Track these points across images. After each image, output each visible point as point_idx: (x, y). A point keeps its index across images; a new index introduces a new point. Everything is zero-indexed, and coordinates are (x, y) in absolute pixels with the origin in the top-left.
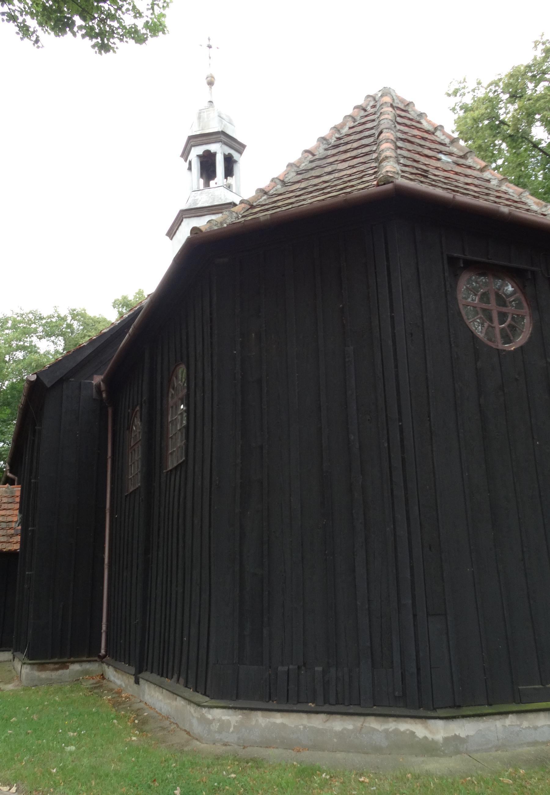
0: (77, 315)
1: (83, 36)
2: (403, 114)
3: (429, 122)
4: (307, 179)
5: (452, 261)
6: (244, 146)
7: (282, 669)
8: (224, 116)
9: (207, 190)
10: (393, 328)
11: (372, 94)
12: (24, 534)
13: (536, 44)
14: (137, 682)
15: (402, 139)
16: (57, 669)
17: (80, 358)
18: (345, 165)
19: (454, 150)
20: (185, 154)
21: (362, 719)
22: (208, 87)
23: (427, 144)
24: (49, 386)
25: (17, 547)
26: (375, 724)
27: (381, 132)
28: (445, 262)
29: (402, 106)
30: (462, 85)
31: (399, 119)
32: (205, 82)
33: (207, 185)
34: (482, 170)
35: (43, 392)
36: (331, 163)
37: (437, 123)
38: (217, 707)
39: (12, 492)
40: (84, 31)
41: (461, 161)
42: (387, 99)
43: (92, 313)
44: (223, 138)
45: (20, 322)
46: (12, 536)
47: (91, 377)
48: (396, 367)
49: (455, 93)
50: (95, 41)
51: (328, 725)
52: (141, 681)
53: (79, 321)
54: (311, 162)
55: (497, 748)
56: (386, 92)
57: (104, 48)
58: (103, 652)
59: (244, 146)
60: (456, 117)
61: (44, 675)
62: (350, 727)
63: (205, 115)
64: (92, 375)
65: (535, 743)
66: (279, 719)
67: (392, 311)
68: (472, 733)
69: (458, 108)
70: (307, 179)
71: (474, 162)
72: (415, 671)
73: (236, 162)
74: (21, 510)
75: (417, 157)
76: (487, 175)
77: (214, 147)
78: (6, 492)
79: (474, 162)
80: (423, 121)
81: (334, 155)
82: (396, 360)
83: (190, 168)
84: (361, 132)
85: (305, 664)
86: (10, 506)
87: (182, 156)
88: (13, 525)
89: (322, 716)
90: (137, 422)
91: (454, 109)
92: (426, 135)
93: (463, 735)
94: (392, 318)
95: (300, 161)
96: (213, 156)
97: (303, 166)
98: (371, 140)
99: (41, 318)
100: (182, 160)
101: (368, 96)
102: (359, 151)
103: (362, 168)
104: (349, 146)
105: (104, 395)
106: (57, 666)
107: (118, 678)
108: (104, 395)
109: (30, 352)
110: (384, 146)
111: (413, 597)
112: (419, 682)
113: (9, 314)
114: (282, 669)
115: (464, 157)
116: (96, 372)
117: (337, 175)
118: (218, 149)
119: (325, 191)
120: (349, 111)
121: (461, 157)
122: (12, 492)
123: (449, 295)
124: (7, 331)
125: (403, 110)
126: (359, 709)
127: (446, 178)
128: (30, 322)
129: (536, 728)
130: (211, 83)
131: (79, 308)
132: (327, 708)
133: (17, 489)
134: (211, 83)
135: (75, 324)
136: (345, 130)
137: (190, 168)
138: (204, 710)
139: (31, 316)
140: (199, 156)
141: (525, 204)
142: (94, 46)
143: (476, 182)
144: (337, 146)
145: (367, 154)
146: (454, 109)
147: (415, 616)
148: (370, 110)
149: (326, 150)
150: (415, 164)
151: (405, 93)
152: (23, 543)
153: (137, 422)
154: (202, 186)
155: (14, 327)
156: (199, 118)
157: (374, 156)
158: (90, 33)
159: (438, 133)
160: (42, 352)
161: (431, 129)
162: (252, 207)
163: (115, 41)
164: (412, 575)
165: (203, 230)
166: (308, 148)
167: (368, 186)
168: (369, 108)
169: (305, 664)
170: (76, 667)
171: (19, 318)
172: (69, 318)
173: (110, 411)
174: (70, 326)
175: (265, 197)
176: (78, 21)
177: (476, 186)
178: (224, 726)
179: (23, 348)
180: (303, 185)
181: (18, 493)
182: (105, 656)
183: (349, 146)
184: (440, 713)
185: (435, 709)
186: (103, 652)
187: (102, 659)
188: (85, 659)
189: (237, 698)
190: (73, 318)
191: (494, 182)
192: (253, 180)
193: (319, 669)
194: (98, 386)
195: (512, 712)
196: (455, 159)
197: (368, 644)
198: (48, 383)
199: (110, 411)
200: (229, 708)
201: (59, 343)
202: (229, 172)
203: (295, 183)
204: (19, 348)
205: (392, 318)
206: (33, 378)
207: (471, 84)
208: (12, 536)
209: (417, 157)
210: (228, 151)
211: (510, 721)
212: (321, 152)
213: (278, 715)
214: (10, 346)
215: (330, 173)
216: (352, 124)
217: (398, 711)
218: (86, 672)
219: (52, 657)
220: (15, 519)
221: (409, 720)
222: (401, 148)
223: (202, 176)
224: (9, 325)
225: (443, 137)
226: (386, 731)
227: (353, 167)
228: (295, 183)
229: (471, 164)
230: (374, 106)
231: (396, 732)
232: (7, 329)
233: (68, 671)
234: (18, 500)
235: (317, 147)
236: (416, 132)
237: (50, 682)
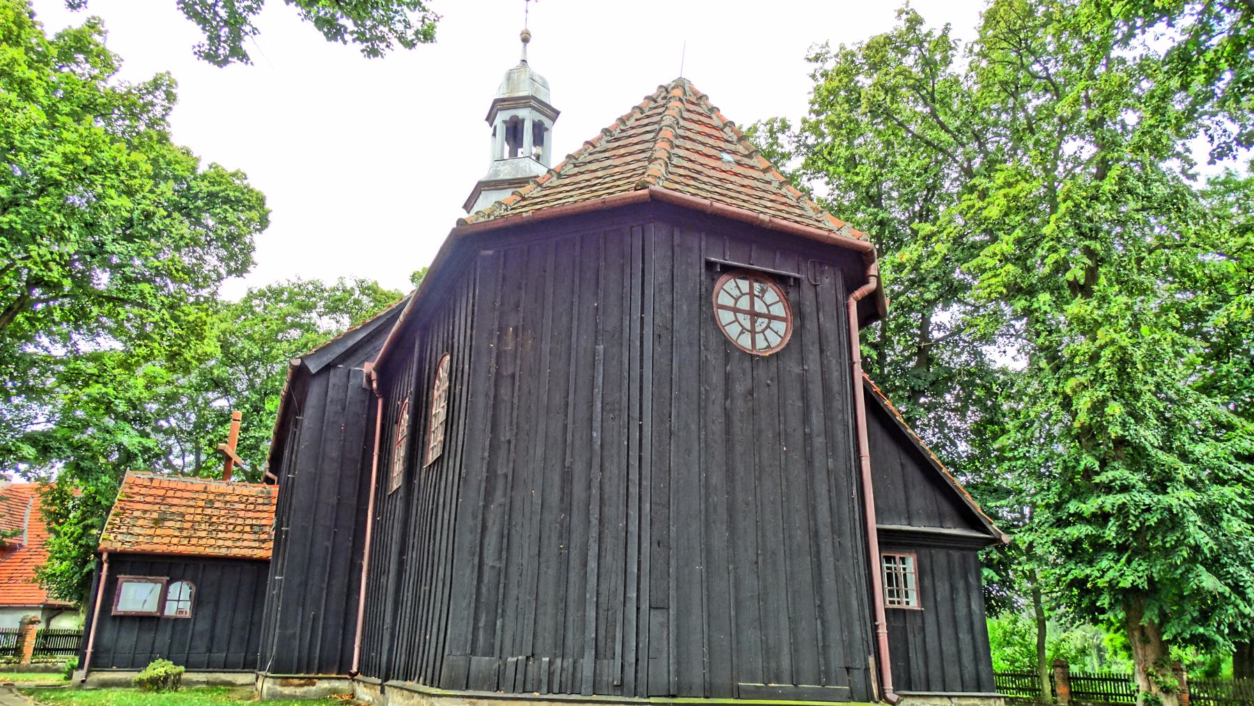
0: (368, 288)
1: (354, 40)
2: (692, 107)
6: (558, 113)
7: (511, 660)
8: (537, 78)
11: (664, 84)
13: (900, 13)
20: (490, 118)
22: (522, 44)
28: (703, 266)
29: (694, 99)
31: (686, 115)
32: (519, 39)
33: (514, 154)
36: (608, 158)
39: (269, 493)
41: (746, 161)
43: (386, 286)
44: (533, 103)
46: (264, 541)
47: (361, 364)
48: (641, 367)
49: (816, 59)
53: (368, 295)
57: (373, 52)
58: (355, 669)
59: (558, 113)
63: (515, 76)
64: (363, 362)
67: (642, 313)
72: (634, 661)
73: (547, 129)
77: (522, 113)
81: (614, 149)
83: (494, 135)
86: (265, 508)
87: (487, 119)
88: (267, 529)
91: (813, 76)
94: (642, 319)
96: (521, 118)
98: (651, 136)
101: (661, 87)
102: (638, 147)
104: (630, 140)
105: (375, 385)
108: (375, 385)
109: (307, 331)
112: (636, 672)
113: (285, 284)
114: (511, 660)
123: (705, 301)
124: (282, 305)
125: (693, 103)
127: (720, 180)
130: (525, 40)
134: (525, 40)
136: (631, 123)
137: (494, 135)
139: (310, 287)
140: (504, 122)
141: (802, 209)
142: (363, 51)
147: (638, 609)
152: (276, 549)
154: (506, 156)
157: (648, 154)
158: (361, 37)
164: (639, 569)
173: (380, 402)
176: (348, 23)
179: (300, 326)
182: (356, 674)
186: (355, 669)
190: (363, 293)
196: (739, 158)
198: (313, 368)
199: (380, 402)
202: (539, 139)
205: (642, 319)
207: (834, 49)
208: (264, 541)
210: (538, 117)
212: (603, 145)
214: (285, 323)
215: (604, 169)
216: (640, 116)
218: (334, 691)
223: (507, 140)
224: (285, 296)
227: (628, 164)
228: (569, 176)
230: (665, 98)
233: (314, 688)
234: (275, 501)
235: (599, 139)
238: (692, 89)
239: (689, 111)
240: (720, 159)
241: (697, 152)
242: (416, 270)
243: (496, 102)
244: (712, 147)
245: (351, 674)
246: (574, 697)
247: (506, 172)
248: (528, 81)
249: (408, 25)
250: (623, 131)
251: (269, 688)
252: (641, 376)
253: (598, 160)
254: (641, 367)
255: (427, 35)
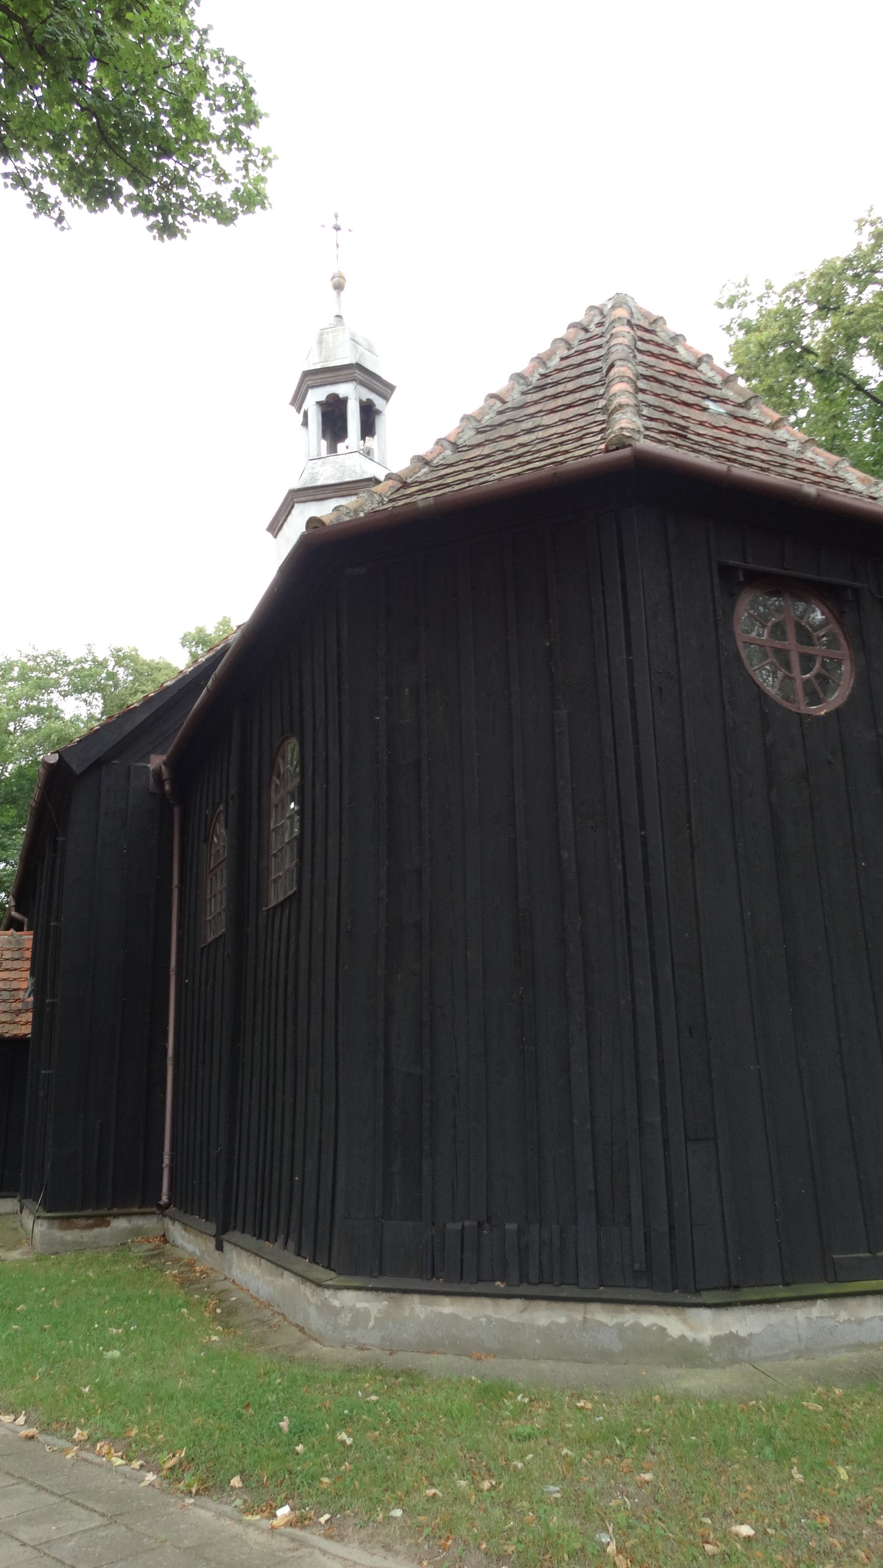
0: (124, 658)
2: (647, 336)
3: (689, 349)
4: (493, 441)
5: (726, 572)
6: (392, 388)
7: (453, 1226)
8: (360, 340)
9: (332, 458)
10: (631, 678)
12: (38, 1009)
13: (861, 224)
14: (219, 1247)
15: (645, 377)
16: (91, 1227)
17: (128, 728)
18: (555, 417)
19: (730, 394)
20: (298, 400)
21: (580, 1307)
23: (686, 384)
24: (78, 773)
25: (27, 1030)
26: (602, 1316)
27: (612, 366)
28: (715, 573)
30: (742, 290)
32: (330, 285)
33: (332, 449)
34: (774, 426)
35: (69, 782)
36: (532, 416)
37: (703, 350)
38: (348, 1288)
39: (19, 942)
40: (135, 204)
41: (741, 412)
42: (622, 313)
43: (149, 654)
44: (358, 374)
45: (32, 670)
46: (18, 1012)
47: (146, 758)
48: (636, 742)
49: (731, 302)
50: (152, 219)
51: (526, 1317)
52: (227, 1246)
53: (127, 667)
54: (500, 413)
55: (799, 1354)
56: (619, 301)
57: (168, 230)
58: (165, 1199)
59: (392, 388)
60: (732, 340)
61: (71, 1235)
62: (562, 1320)
63: (329, 338)
65: (858, 1346)
66: (447, 1307)
67: (629, 651)
68: (756, 1330)
69: (735, 327)
70: (493, 441)
71: (761, 413)
72: (666, 1229)
73: (379, 412)
74: (33, 971)
75: (670, 406)
76: (781, 434)
77: (343, 390)
78: (9, 942)
79: (761, 413)
80: (678, 348)
81: (536, 402)
82: (635, 731)
83: (305, 423)
84: (580, 365)
85: (489, 1220)
86: (16, 964)
87: (293, 403)
88: (21, 995)
89: (517, 1303)
90: (221, 830)
91: (728, 329)
92: (684, 371)
93: (743, 1333)
94: (630, 663)
95: (482, 411)
97: (486, 420)
98: (596, 377)
99: (66, 663)
100: (293, 409)
101: (592, 308)
102: (577, 396)
103: (581, 422)
104: (560, 388)
105: (167, 787)
106: (90, 1222)
107: (189, 1241)
108: (167, 787)
109: (49, 718)
110: (617, 388)
111: (664, 1109)
112: (672, 1247)
113: (15, 657)
114: (453, 1226)
115: (745, 405)
116: (154, 750)
117: (541, 434)
118: (351, 393)
119: (522, 460)
120: (561, 332)
121: (740, 405)
122: (19, 942)
124: (11, 684)
126: (575, 1291)
127: (716, 439)
128: (48, 670)
129: (860, 1322)
130: (339, 287)
131: (126, 647)
132: (525, 1289)
133: (27, 938)
134: (339, 287)
135: (121, 673)
136: (554, 363)
137: (305, 423)
138: (328, 1293)
139: (49, 659)
140: (319, 404)
141: (843, 480)
142: (151, 228)
143: (765, 445)
144: (542, 388)
145: (589, 401)
146: (728, 329)
148: (594, 330)
149: (524, 393)
150: (666, 417)
151: (650, 302)
152: (37, 1024)
153: (221, 830)
154: (324, 451)
155: (23, 677)
156: (320, 342)
157: (601, 403)
158: (145, 207)
159: (703, 367)
160: (67, 717)
161: (692, 360)
162: (405, 485)
163: (185, 220)
164: (662, 1075)
165: (327, 521)
166: (494, 391)
167: (591, 451)
168: (592, 327)
169: (489, 1220)
170: (121, 1224)
171: (31, 663)
172: (111, 663)
173: (177, 811)
174: (112, 676)
175: (426, 470)
177: (764, 452)
178: (359, 1318)
179: (38, 711)
180: (486, 450)
181: (29, 944)
182: (167, 1206)
183: (560, 388)
184: (706, 1297)
185: (698, 1291)
186: (165, 1199)
187: (163, 1210)
188: (136, 1210)
189: (381, 1272)
190: (118, 663)
191: (793, 446)
192: (408, 441)
193: (512, 1226)
194: (158, 773)
195: (822, 1297)
196: (730, 408)
197: (591, 1187)
198: (77, 768)
199: (177, 811)
200: (367, 1289)
201: (94, 702)
202: (368, 429)
203: (473, 447)
204: (30, 711)
205: (630, 663)
206: (53, 759)
208: (18, 1012)
209: (670, 406)
210: (366, 395)
211: (819, 1309)
212: (516, 397)
213: (447, 1300)
214: (17, 708)
215: (529, 431)
216: (566, 353)
217: (639, 1295)
218: (137, 1232)
219: (83, 1208)
220: (24, 985)
221: (656, 1309)
222: (643, 391)
223: (324, 436)
224: (15, 674)
225: (711, 374)
226: (620, 1327)
228: (473, 447)
229: (757, 417)
230: (600, 324)
231: (636, 1327)
232: (12, 680)
233: (108, 1229)
234: (28, 954)
235: (510, 390)
236: (668, 366)
237: (80, 1248)
238: (639, 309)
239: (642, 340)
240: (705, 409)
241: (672, 400)
242: (186, 631)
243: (307, 374)
244: (691, 392)
245: (159, 1207)
246: (565, 1291)
247: (329, 472)
248: (349, 344)
249: (222, 176)
250: (544, 376)
251: (43, 1234)
252: (637, 756)
253: (514, 421)
254: (636, 742)
255: (251, 199)
